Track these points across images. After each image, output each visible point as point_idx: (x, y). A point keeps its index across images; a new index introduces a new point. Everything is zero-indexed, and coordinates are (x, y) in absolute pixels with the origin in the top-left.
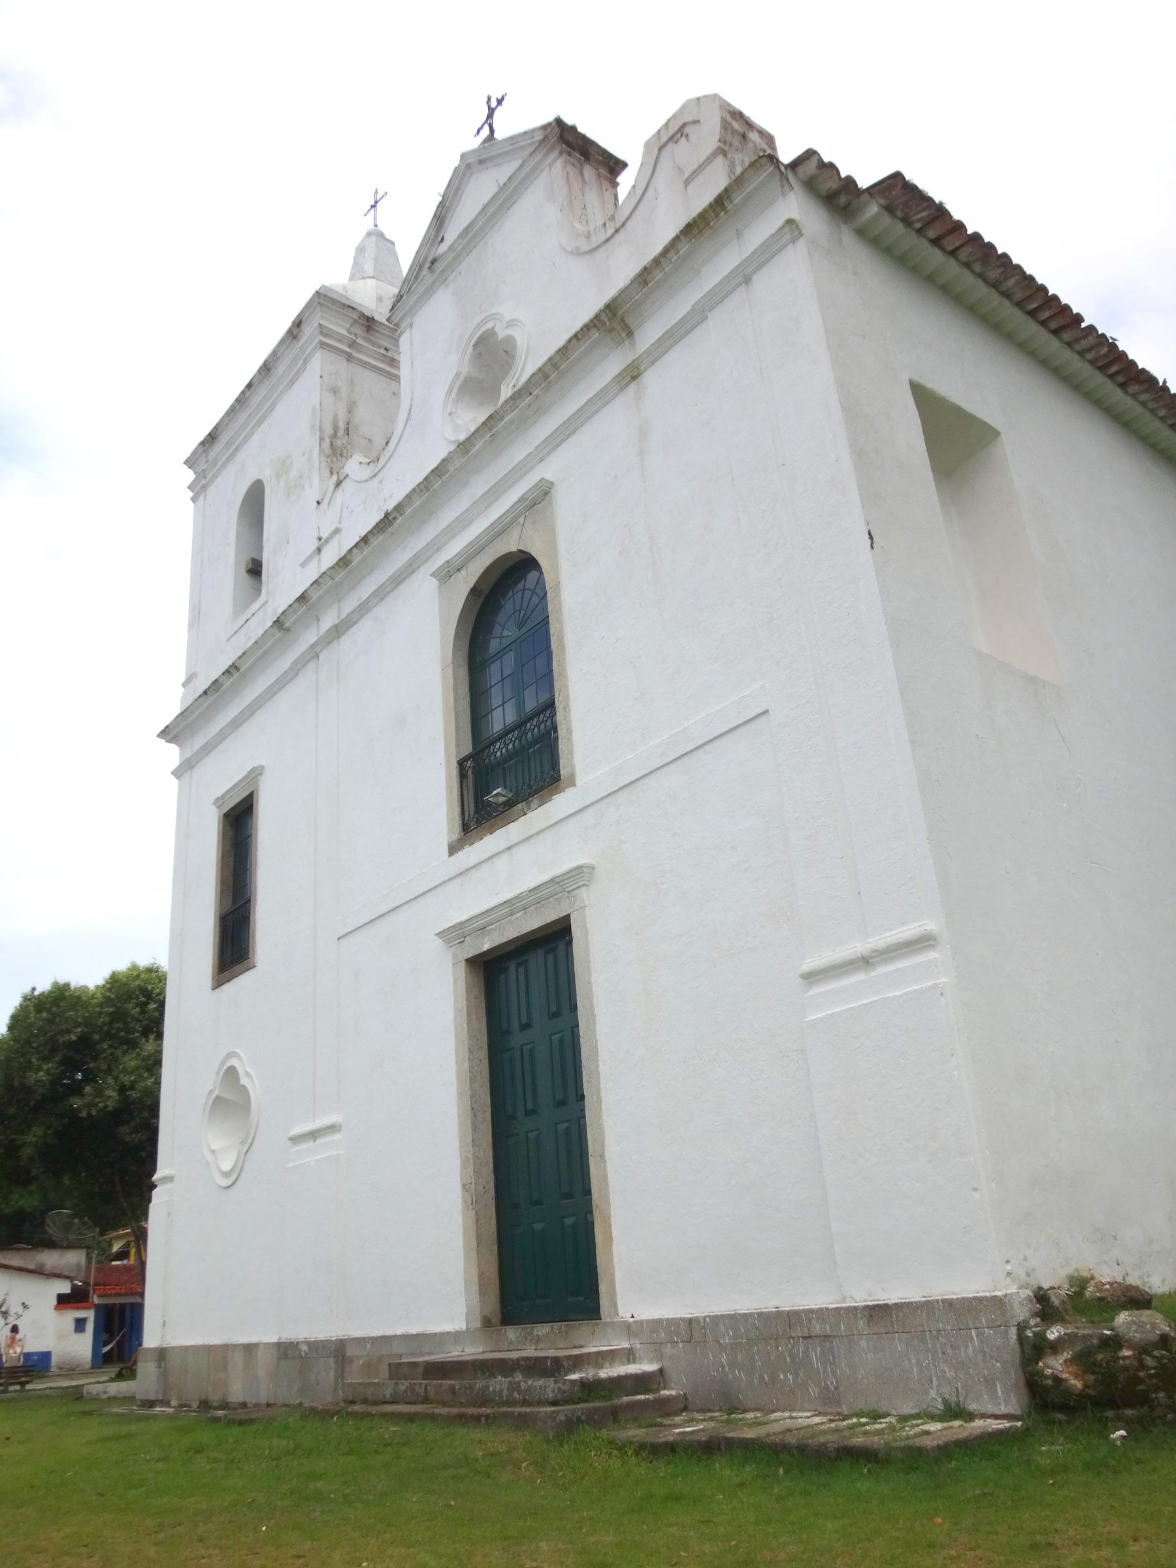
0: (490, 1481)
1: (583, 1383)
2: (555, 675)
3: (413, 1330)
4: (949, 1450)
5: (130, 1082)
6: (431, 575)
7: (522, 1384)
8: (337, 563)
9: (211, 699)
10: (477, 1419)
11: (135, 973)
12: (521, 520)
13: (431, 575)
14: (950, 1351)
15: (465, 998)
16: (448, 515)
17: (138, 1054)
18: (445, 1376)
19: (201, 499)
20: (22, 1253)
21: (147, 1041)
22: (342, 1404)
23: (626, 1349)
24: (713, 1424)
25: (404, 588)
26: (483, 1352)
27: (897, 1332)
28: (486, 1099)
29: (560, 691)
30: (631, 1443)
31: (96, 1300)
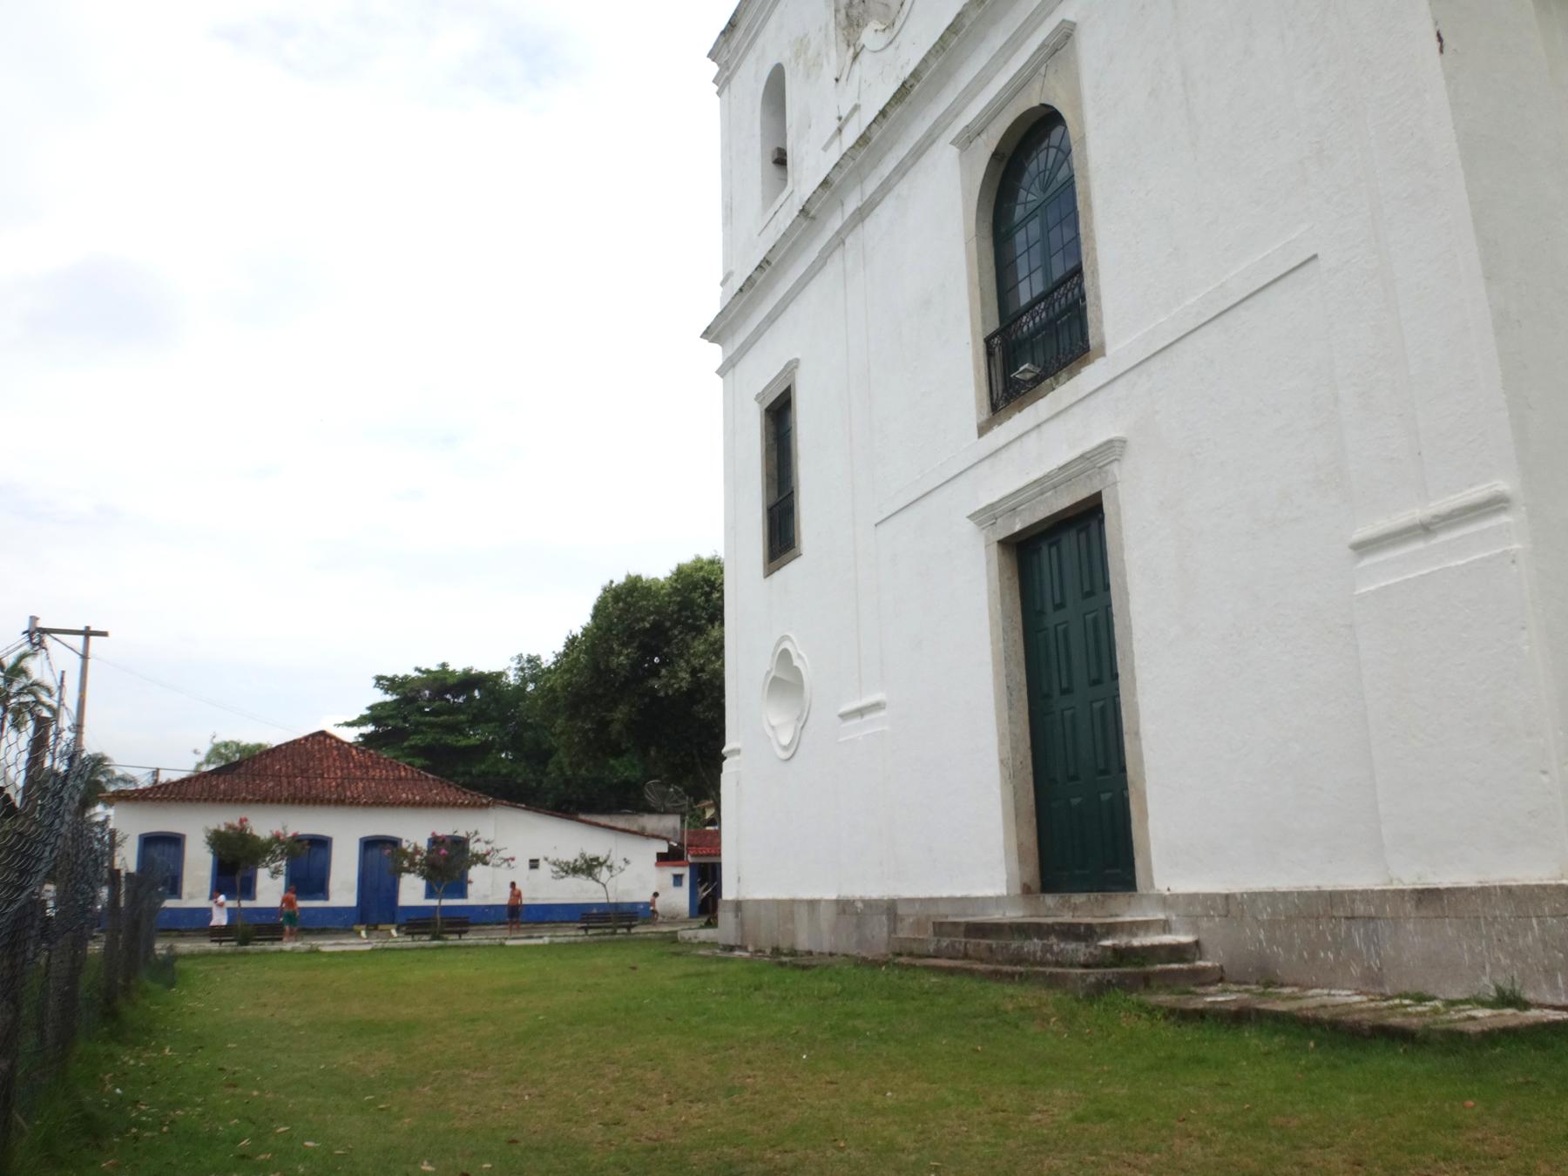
0: (1018, 1032)
1: (1115, 950)
2: (1082, 240)
3: (958, 894)
4: (1492, 1037)
5: (700, 664)
6: (951, 143)
7: (1055, 947)
8: (857, 142)
9: (746, 296)
10: (1011, 976)
11: (699, 565)
12: (1042, 70)
13: (951, 143)
14: (1506, 938)
15: (997, 579)
16: (966, 75)
17: (706, 640)
18: (984, 936)
19: (726, 90)
20: (626, 817)
21: (713, 627)
22: (890, 956)
23: (1160, 920)
24: (1246, 996)
25: (926, 161)
26: (1024, 917)
27: (1447, 917)
28: (1021, 677)
29: (1088, 254)
30: (1161, 1007)
31: (690, 859)
